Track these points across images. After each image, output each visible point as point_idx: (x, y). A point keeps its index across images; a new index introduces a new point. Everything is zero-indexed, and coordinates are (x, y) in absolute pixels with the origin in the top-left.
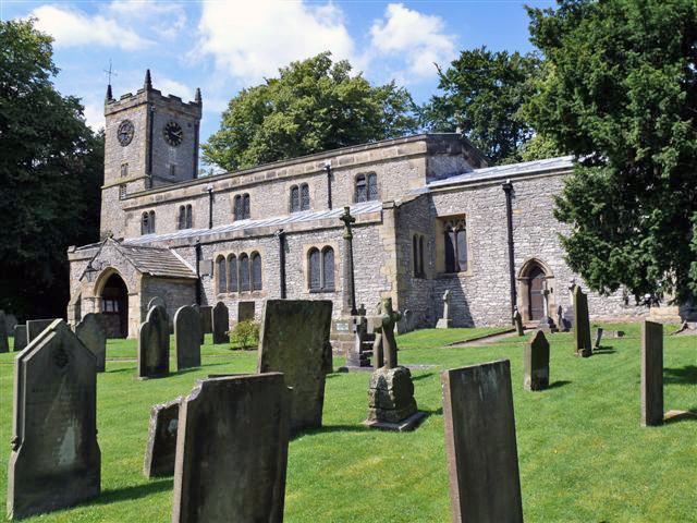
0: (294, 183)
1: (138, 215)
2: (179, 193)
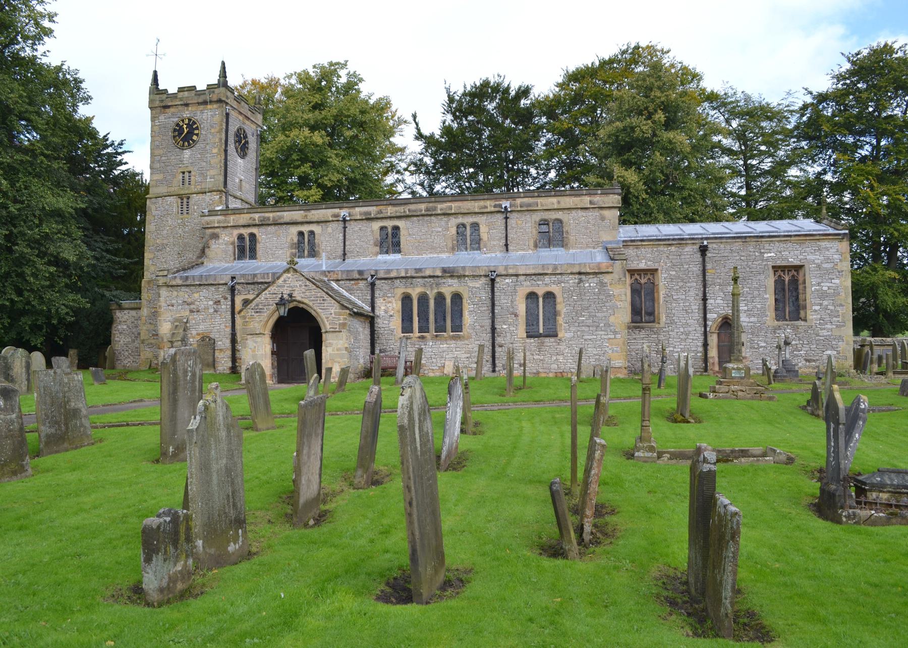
0: (460, 220)
2: (297, 215)
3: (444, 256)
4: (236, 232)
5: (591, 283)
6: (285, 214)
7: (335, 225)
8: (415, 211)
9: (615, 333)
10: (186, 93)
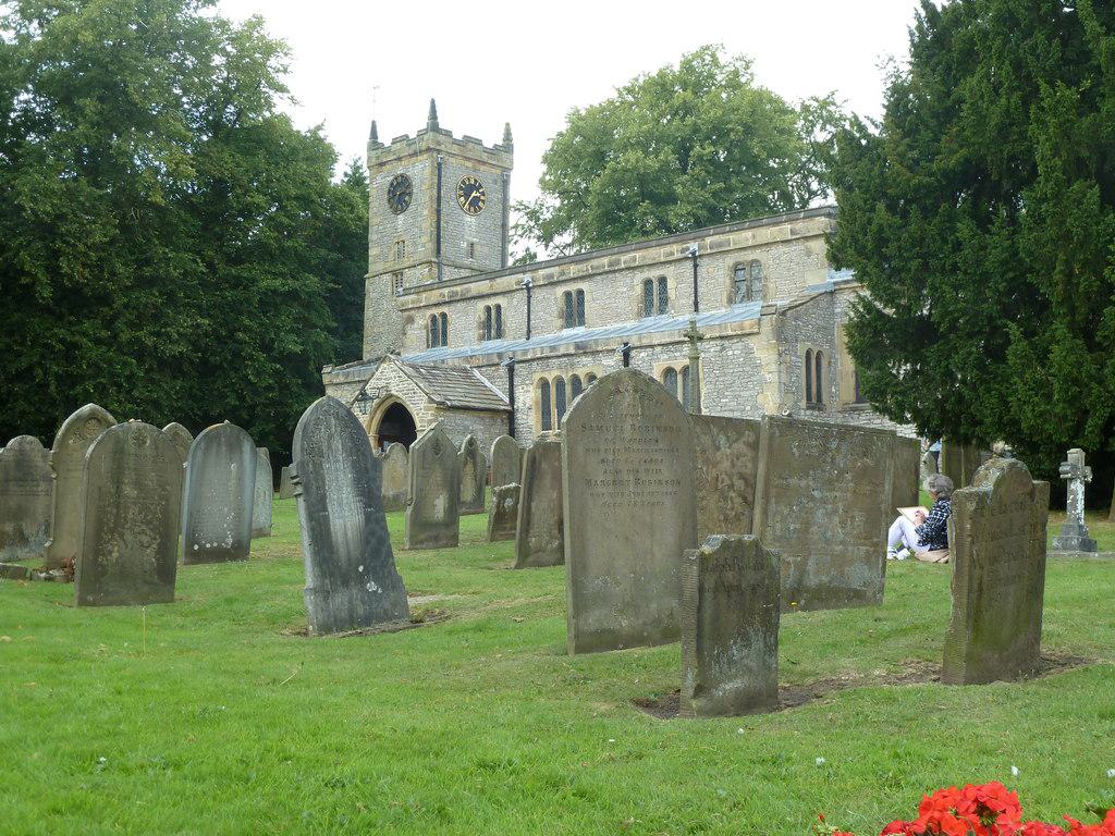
1: (422, 320)
3: (629, 324)
4: (429, 313)
8: (597, 268)
10: (398, 144)
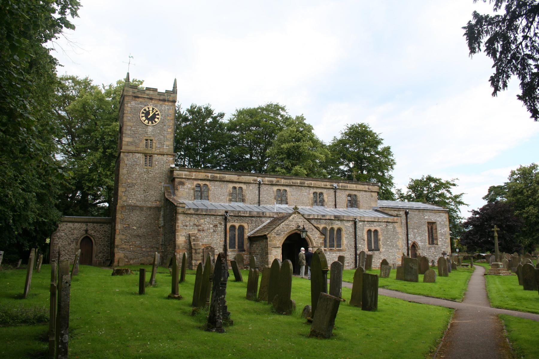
0: (315, 190)
2: (234, 177)
4: (196, 183)
5: (390, 226)
6: (227, 176)
7: (254, 185)
9: (399, 249)
